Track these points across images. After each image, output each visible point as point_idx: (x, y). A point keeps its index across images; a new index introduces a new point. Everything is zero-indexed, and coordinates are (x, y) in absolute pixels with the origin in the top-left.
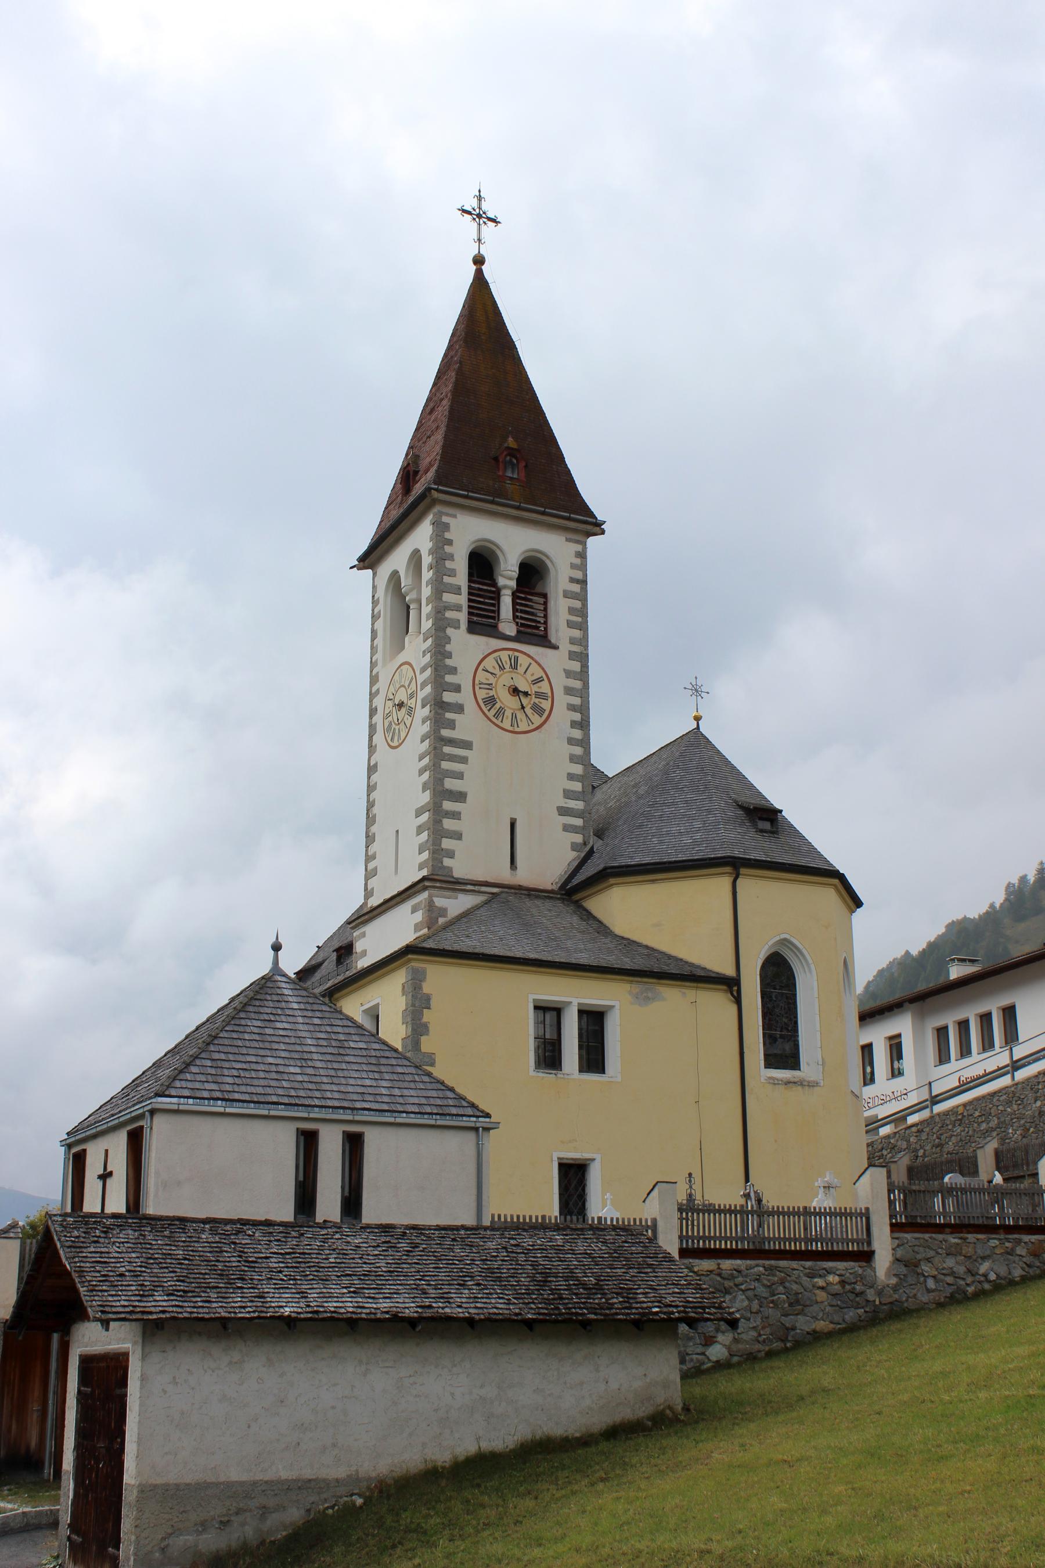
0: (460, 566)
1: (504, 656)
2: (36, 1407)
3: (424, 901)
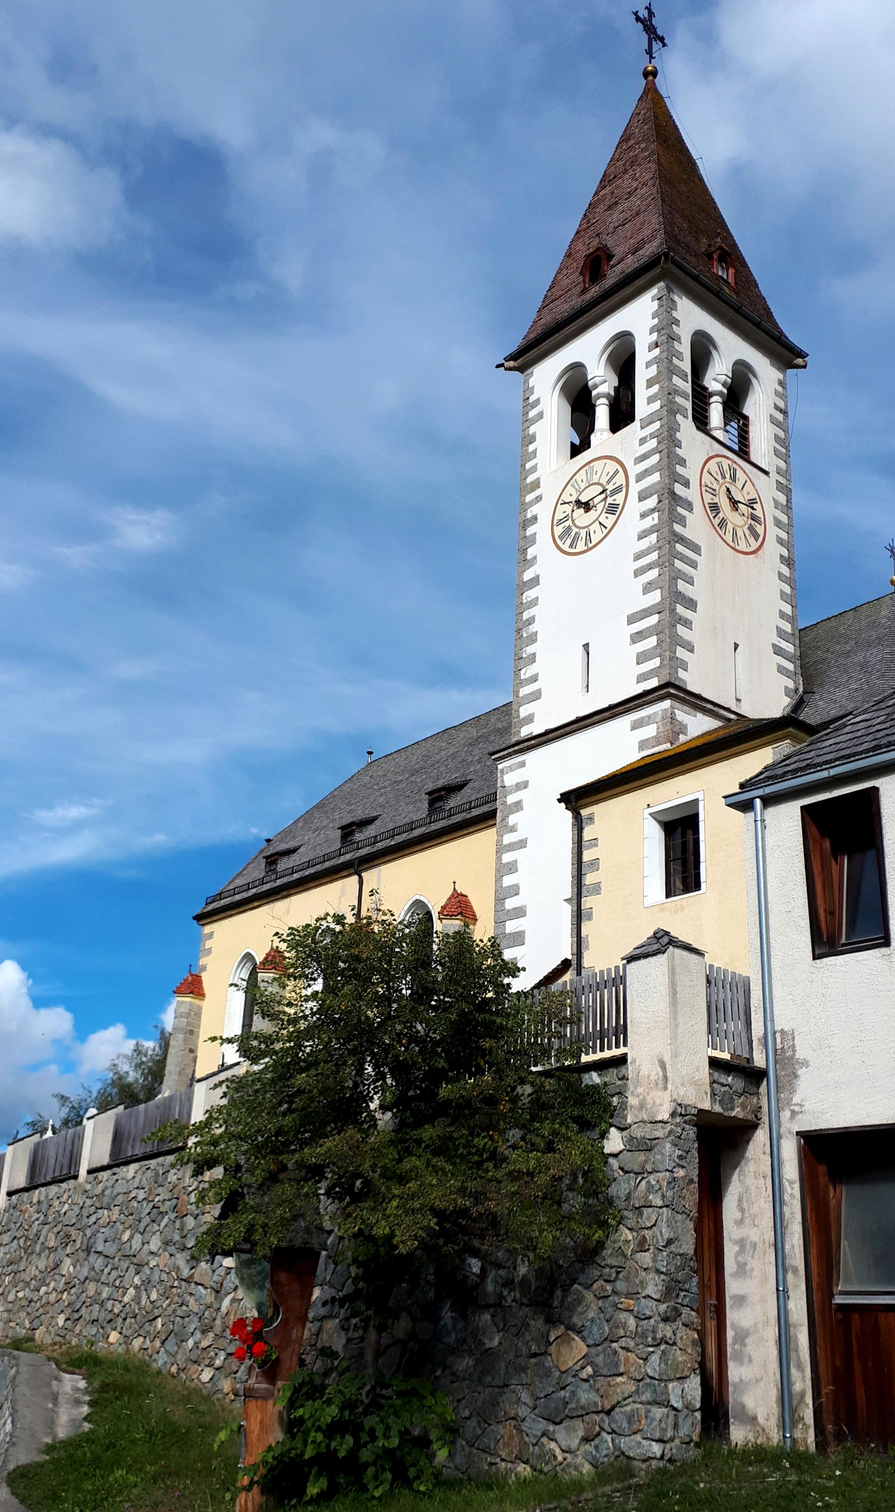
0: (685, 348)
1: (725, 463)
2: (814, 1285)
3: (660, 713)
